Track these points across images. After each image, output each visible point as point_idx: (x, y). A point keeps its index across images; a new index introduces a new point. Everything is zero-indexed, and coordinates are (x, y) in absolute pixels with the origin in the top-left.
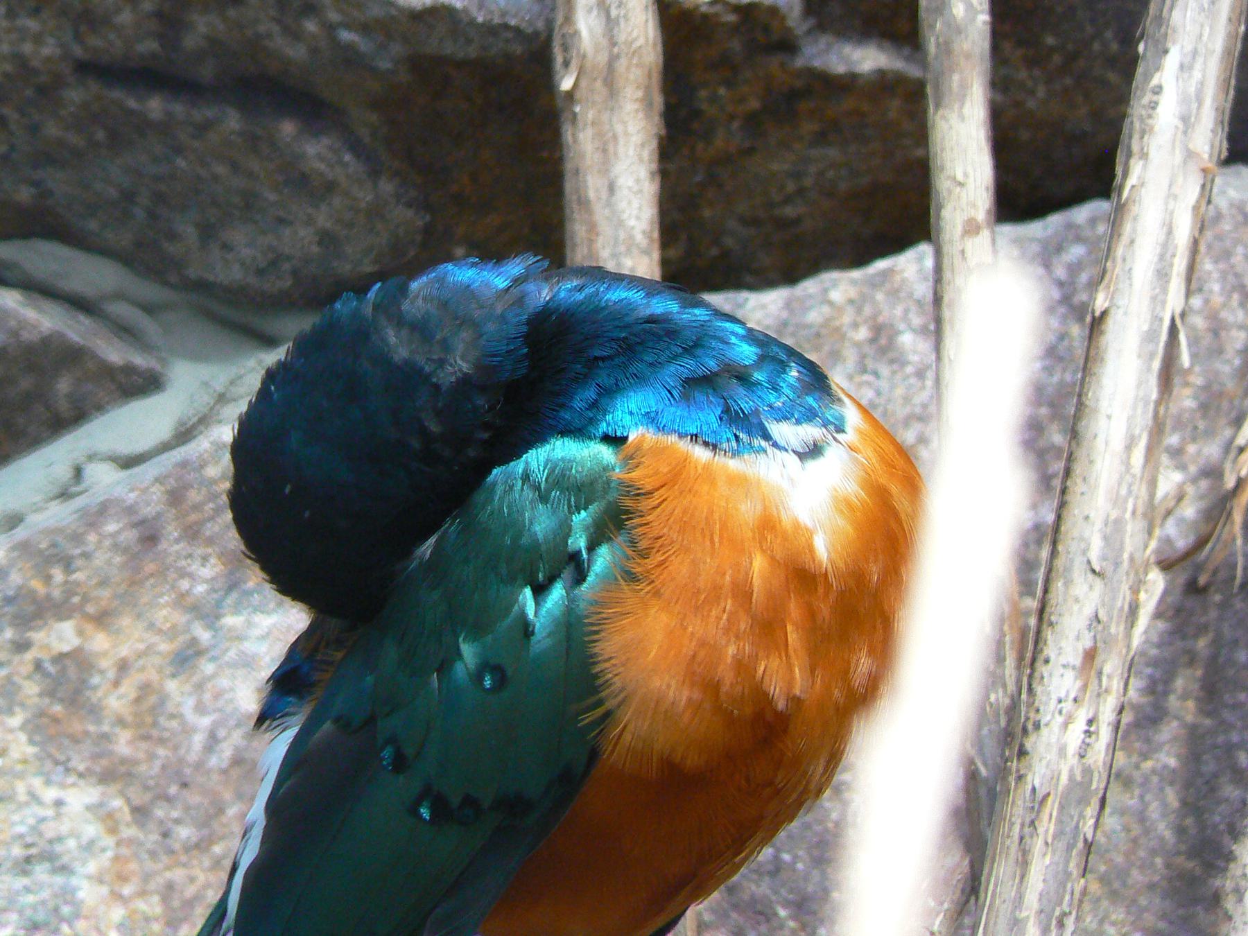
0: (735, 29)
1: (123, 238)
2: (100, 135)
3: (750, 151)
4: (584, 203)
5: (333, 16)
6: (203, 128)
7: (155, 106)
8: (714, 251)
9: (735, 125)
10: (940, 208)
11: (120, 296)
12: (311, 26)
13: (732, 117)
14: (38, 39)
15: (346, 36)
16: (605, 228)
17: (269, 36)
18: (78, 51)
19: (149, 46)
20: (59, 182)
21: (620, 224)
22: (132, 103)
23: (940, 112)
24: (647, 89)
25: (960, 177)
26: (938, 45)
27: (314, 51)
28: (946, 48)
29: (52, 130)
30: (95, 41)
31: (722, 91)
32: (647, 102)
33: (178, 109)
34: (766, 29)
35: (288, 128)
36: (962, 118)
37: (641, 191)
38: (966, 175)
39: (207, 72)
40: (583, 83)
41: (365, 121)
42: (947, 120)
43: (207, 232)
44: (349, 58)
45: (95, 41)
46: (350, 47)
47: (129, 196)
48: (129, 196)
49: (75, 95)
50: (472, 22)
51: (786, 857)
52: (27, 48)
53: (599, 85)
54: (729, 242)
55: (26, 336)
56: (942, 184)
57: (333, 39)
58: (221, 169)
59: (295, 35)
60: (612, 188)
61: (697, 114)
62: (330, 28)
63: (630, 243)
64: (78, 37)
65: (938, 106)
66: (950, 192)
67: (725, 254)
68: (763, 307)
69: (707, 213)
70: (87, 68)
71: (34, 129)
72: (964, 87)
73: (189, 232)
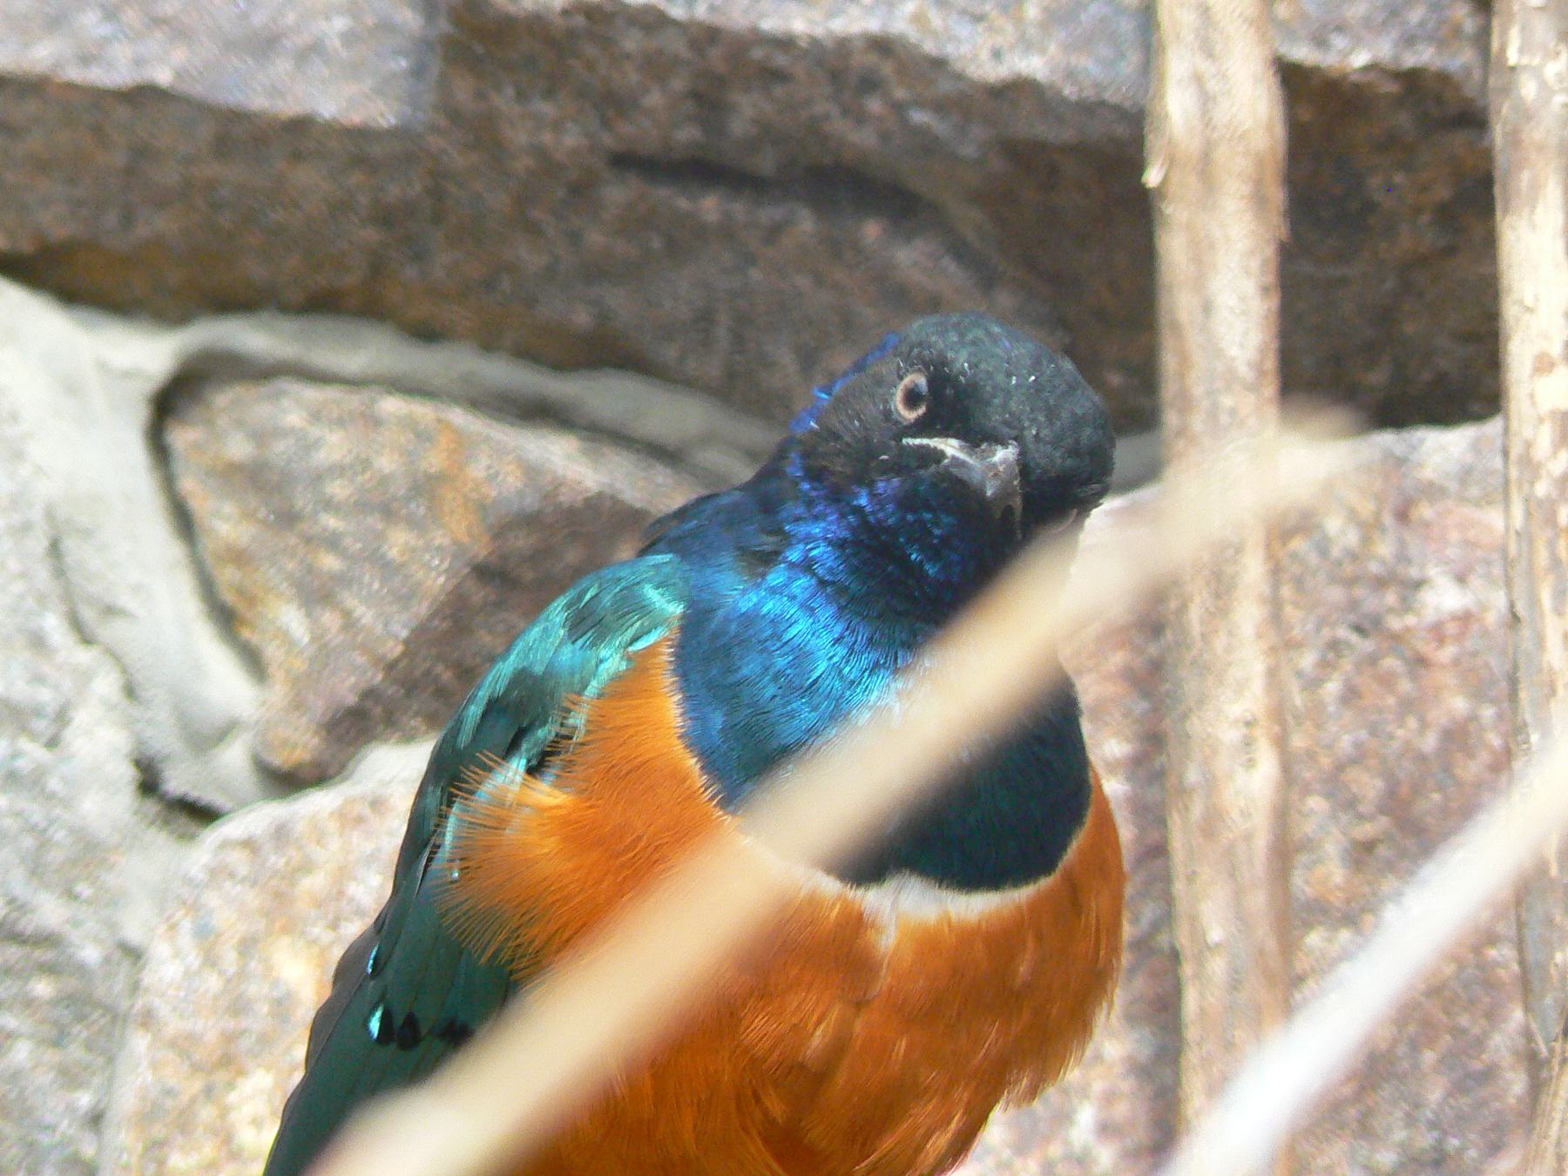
0: (1399, 102)
1: (713, 369)
2: (656, 243)
3: (1451, 251)
4: (1176, 327)
5: (900, 93)
6: (773, 233)
7: (710, 206)
8: (1426, 376)
9: (1425, 218)
10: (1508, 339)
11: (707, 439)
12: (874, 105)
13: (1418, 211)
14: (557, 126)
15: (919, 117)
16: (1199, 360)
17: (827, 117)
18: (608, 140)
19: (687, 134)
20: (620, 301)
21: (1218, 353)
22: (683, 203)
23: (1508, 219)
24: (1258, 183)
25: (1529, 302)
26: (1505, 135)
27: (885, 137)
28: (1514, 139)
29: (595, 238)
30: (625, 128)
31: (1399, 178)
32: (1258, 200)
33: (739, 209)
34: (1439, 100)
35: (871, 230)
36: (1533, 227)
37: (1244, 313)
38: (1537, 299)
39: (766, 163)
40: (1175, 179)
41: (970, 220)
42: (1514, 229)
43: (808, 360)
44: (927, 145)
45: (625, 128)
46: (922, 132)
47: (705, 318)
48: (705, 318)
49: (618, 193)
50: (1064, 101)
51: (1454, 1143)
52: (547, 138)
53: (1193, 180)
54: (1444, 364)
55: (565, 498)
56: (1510, 310)
57: (904, 122)
58: (803, 281)
59: (861, 118)
60: (1207, 308)
61: (1370, 207)
62: (899, 108)
63: (1230, 378)
64: (606, 123)
65: (1506, 211)
66: (1518, 320)
67: (1441, 378)
68: (1443, 448)
69: (1409, 329)
70: (625, 161)
71: (574, 238)
72: (1536, 187)
73: (785, 358)
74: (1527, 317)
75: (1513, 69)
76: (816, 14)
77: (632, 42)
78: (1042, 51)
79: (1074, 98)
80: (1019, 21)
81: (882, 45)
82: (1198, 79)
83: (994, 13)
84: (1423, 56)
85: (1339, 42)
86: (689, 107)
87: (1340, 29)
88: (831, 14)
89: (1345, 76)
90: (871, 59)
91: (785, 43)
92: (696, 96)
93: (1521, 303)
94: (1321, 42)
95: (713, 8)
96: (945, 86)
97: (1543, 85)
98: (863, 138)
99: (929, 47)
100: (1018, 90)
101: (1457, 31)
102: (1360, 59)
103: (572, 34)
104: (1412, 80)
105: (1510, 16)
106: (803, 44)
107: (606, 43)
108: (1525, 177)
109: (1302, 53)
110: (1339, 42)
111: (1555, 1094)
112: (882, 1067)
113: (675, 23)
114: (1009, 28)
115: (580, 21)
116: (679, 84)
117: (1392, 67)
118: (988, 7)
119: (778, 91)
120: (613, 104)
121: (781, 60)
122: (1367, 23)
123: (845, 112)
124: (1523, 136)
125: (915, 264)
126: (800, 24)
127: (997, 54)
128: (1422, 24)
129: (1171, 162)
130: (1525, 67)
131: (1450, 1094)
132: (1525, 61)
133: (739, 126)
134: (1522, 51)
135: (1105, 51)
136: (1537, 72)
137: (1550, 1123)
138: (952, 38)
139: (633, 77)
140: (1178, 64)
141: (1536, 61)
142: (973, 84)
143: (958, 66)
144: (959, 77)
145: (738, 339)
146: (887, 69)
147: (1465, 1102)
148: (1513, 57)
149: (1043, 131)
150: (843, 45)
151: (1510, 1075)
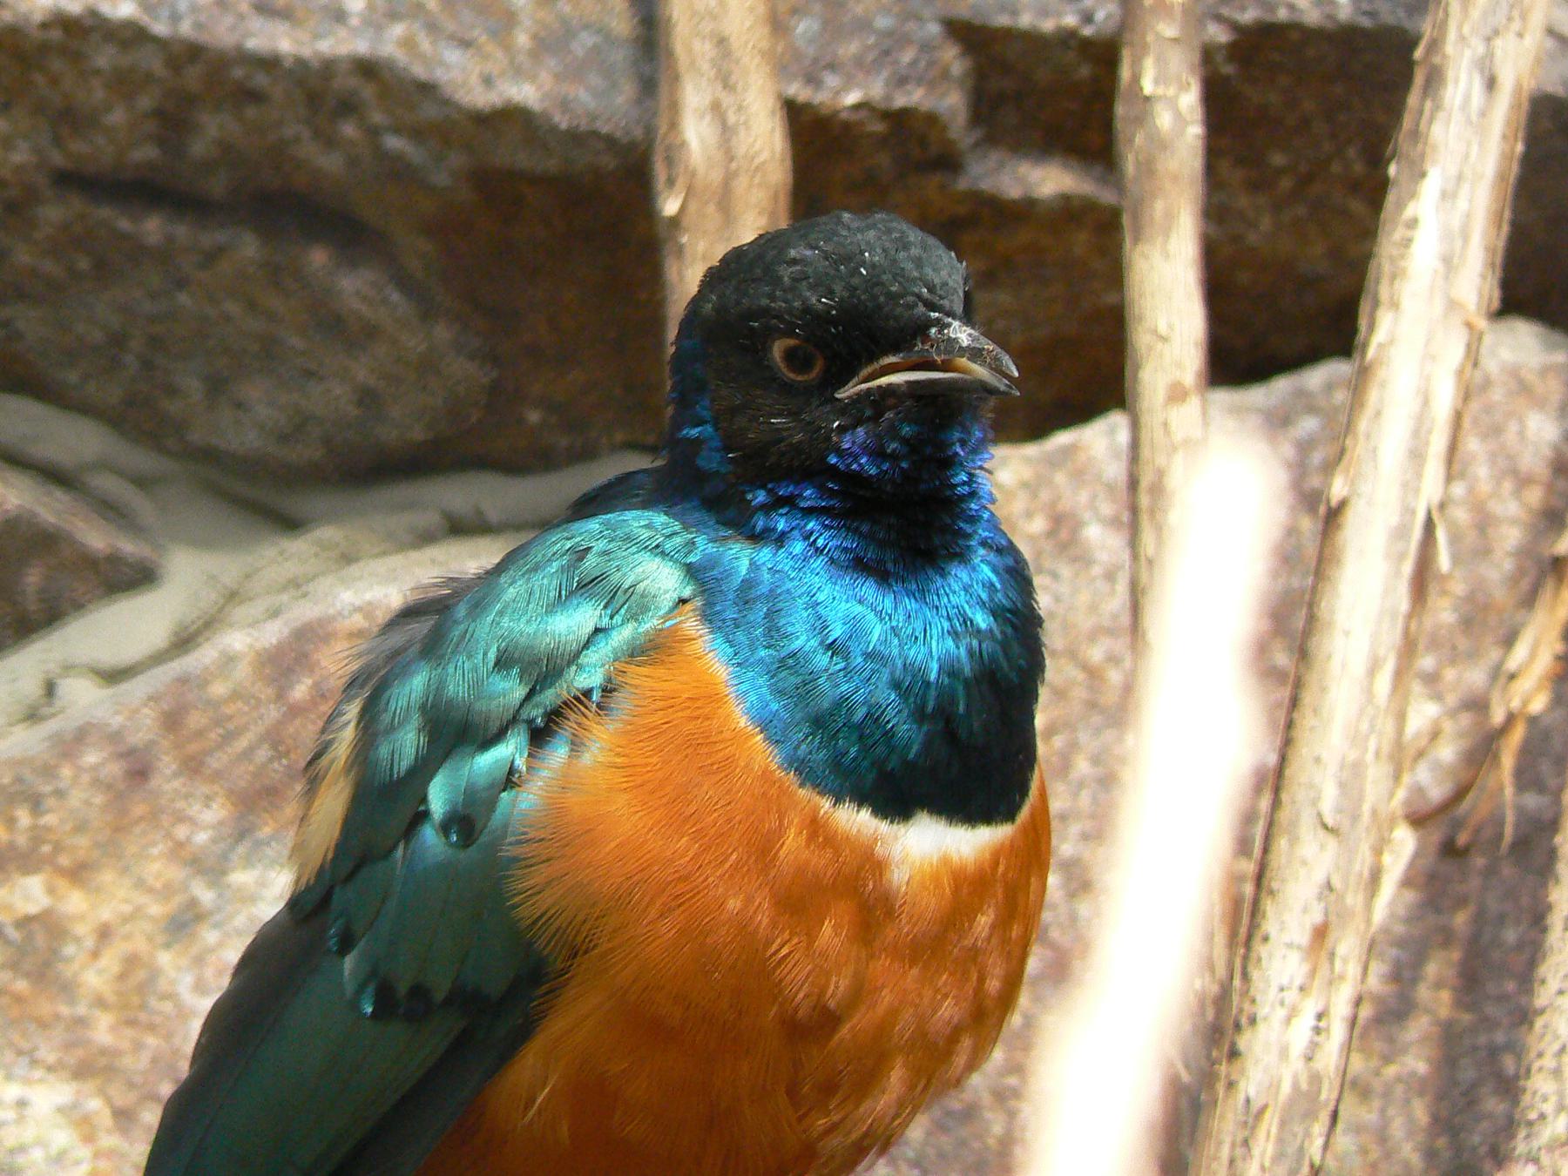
0: (883, 141)
1: (112, 394)
2: (83, 264)
5: (377, 117)
6: (211, 257)
7: (153, 228)
11: (104, 465)
12: (349, 130)
15: (393, 143)
17: (297, 140)
18: (57, 159)
19: (146, 153)
22: (124, 224)
23: (1139, 248)
25: (1162, 328)
26: (1138, 163)
27: (353, 162)
29: (23, 256)
30: (78, 146)
33: (182, 231)
34: (923, 142)
35: (318, 258)
36: (1166, 255)
38: (1170, 327)
39: (217, 186)
40: (693, 207)
41: (416, 249)
42: (1147, 257)
43: (216, 386)
44: (397, 171)
45: (78, 146)
48: (118, 340)
49: (53, 213)
50: (554, 129)
53: (711, 209)
58: (232, 307)
62: (373, 132)
64: (58, 141)
65: (1137, 240)
66: (1150, 348)
70: (69, 180)
72: (1170, 217)
73: (193, 387)
74: (1159, 345)
75: (1147, 99)
76: (303, 36)
77: (104, 58)
78: (533, 78)
79: (564, 126)
80: (507, 47)
81: (367, 68)
82: (716, 108)
83: (483, 39)
84: (912, 97)
85: (831, 80)
86: (150, 126)
87: (832, 67)
88: (317, 36)
89: (836, 113)
90: (353, 82)
91: (269, 63)
92: (159, 113)
93: (1155, 332)
94: (812, 80)
95: (198, 26)
96: (429, 111)
97: (1178, 115)
98: (330, 163)
99: (419, 71)
100: (511, 117)
101: (945, 75)
102: (852, 98)
103: (44, 48)
104: (900, 120)
105: (1144, 49)
106: (287, 64)
107: (76, 58)
108: (1159, 206)
109: (798, 91)
110: (831, 80)
111: (1222, 1117)
112: (905, 1038)
113: (155, 39)
114: (499, 54)
115: (56, 35)
116: (145, 102)
117: (883, 106)
118: (476, 33)
119: (251, 112)
120: (70, 119)
121: (261, 80)
122: (859, 62)
123: (317, 133)
124: (1159, 167)
125: (358, 293)
126: (284, 41)
127: (488, 81)
128: (914, 63)
129: (690, 192)
130: (1160, 98)
131: (929, 1134)
132: (1160, 91)
133: (199, 148)
134: (1157, 82)
135: (595, 80)
136: (1173, 103)
137: (1219, 1144)
138: (442, 63)
139: (99, 94)
140: (694, 96)
141: (1171, 92)
142: (459, 108)
143: (448, 91)
144: (447, 102)
145: (147, 365)
146: (368, 92)
147: (945, 1141)
148: (1148, 87)
149: (524, 160)
150: (328, 67)
151: (988, 1115)
